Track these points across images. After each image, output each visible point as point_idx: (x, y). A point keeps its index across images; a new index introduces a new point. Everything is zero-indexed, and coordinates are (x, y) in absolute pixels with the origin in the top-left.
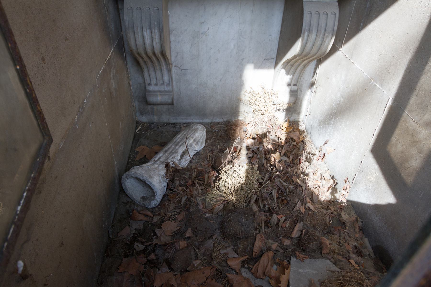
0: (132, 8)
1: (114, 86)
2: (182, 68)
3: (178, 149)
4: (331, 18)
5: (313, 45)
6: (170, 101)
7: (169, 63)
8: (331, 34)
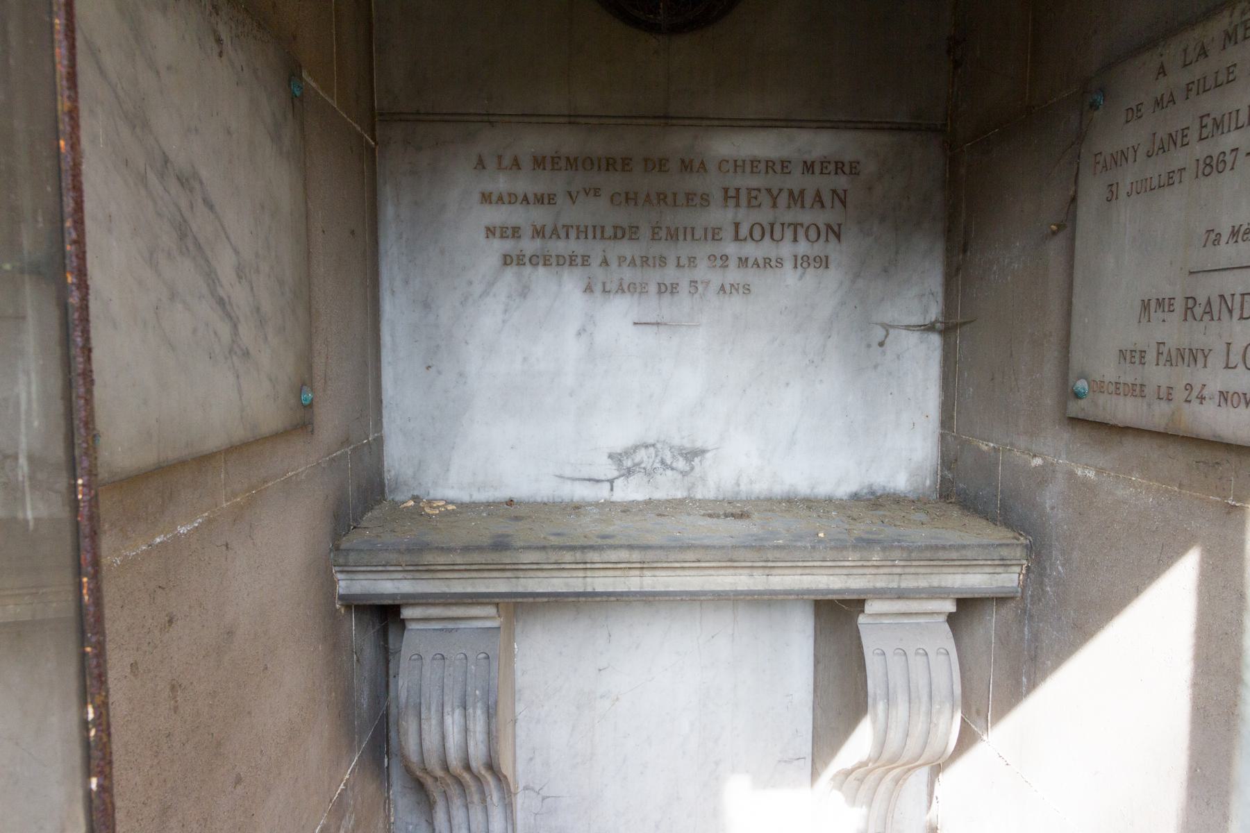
7: (509, 791)
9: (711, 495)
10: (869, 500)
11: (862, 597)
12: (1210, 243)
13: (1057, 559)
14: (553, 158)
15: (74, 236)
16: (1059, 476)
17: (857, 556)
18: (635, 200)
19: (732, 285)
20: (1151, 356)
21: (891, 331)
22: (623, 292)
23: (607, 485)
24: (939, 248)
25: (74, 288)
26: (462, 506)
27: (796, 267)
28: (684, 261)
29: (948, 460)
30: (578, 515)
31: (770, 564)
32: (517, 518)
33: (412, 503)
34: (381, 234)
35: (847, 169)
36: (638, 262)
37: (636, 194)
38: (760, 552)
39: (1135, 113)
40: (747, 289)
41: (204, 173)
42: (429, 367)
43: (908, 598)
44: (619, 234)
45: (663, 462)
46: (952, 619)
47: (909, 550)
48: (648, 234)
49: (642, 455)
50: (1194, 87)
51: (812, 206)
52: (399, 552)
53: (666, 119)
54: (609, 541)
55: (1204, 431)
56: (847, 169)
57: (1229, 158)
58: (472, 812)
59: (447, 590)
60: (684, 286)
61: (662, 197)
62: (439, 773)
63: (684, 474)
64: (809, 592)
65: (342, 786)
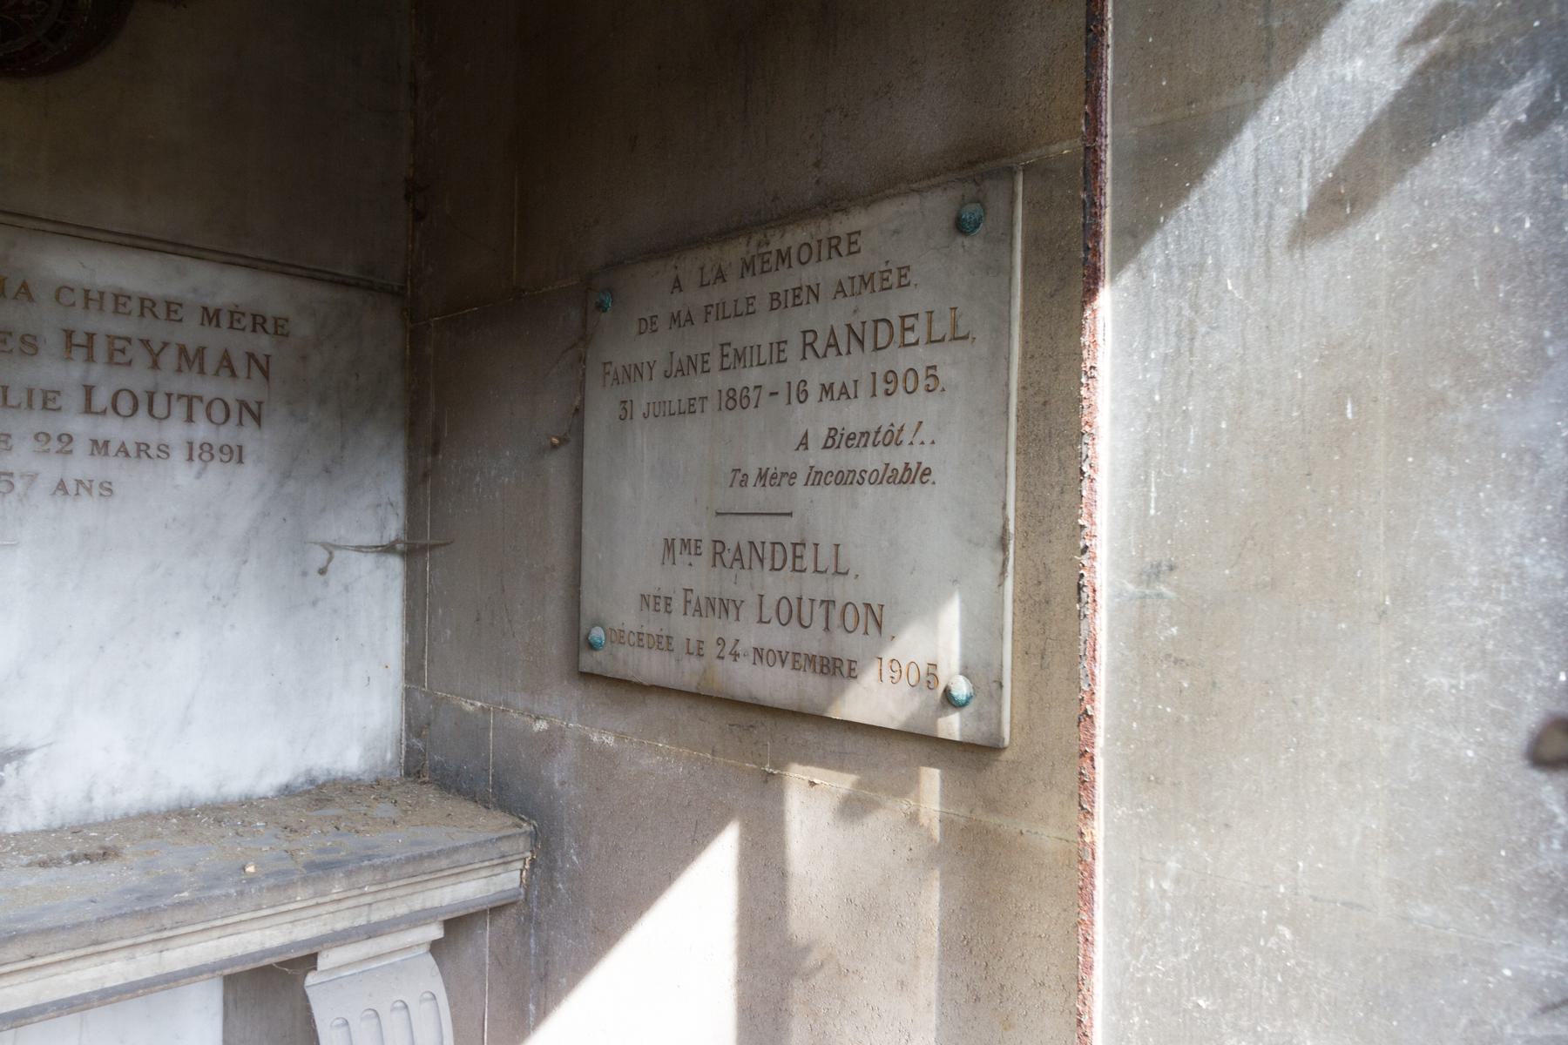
9: (38, 823)
10: (309, 792)
12: (736, 484)
13: (569, 847)
16: (570, 742)
17: (310, 890)
19: (79, 482)
20: (677, 604)
21: (337, 553)
24: (399, 444)
27: (190, 459)
29: (416, 724)
35: (269, 326)
38: (148, 913)
39: (649, 325)
47: (384, 868)
51: (217, 374)
55: (740, 693)
56: (269, 326)
57: (753, 395)
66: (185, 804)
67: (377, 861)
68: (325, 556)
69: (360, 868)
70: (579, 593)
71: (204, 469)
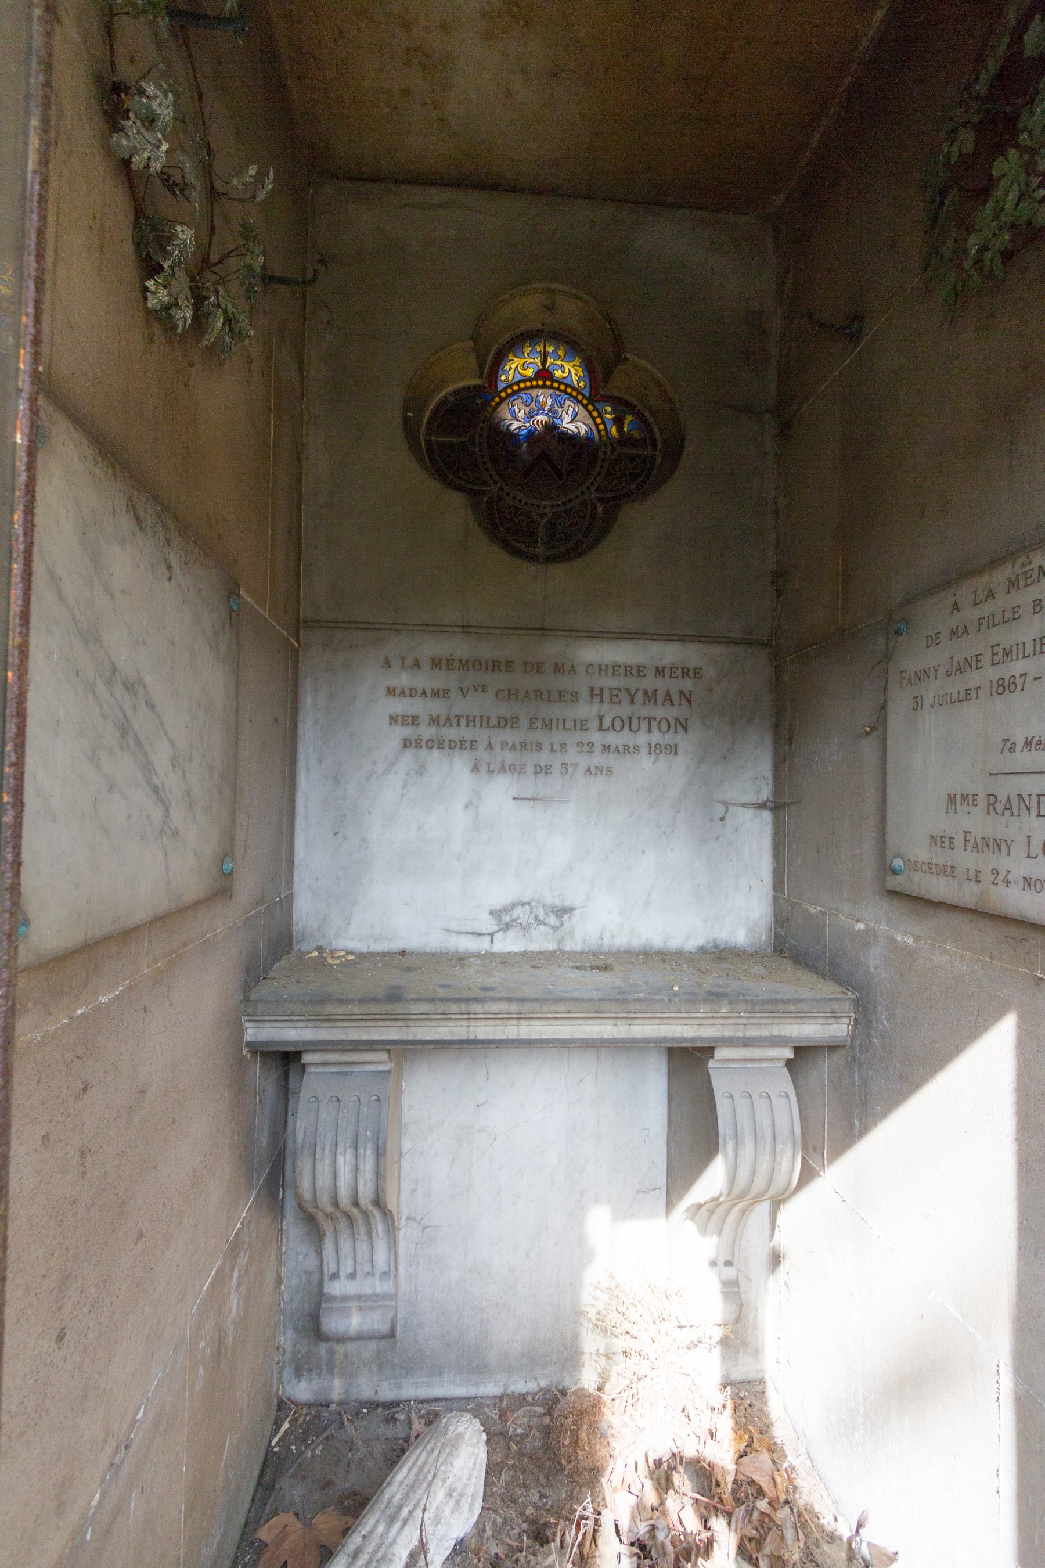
0: (318, 1100)
1: (235, 1308)
2: (425, 1222)
3: (394, 1542)
4: (779, 1104)
5: (754, 1172)
6: (385, 1328)
8: (790, 1145)
9: (578, 947)
10: (714, 953)
11: (713, 1045)
12: (1006, 750)
13: (882, 1014)
14: (448, 660)
15: (13, 758)
17: (708, 1008)
18: (517, 696)
19: (597, 768)
20: (959, 842)
22: (505, 771)
23: (488, 938)
25: (9, 807)
26: (362, 957)
27: (650, 753)
28: (556, 747)
29: (781, 918)
30: (462, 966)
31: (632, 1015)
32: (409, 969)
33: (316, 954)
34: (300, 719)
35: (691, 674)
36: (518, 747)
37: (517, 691)
38: (621, 1003)
39: (934, 640)
40: (610, 771)
41: (148, 679)
42: (336, 834)
43: (752, 1046)
44: (502, 724)
45: (536, 918)
46: (789, 1063)
48: (527, 724)
49: (518, 912)
50: (985, 622)
52: (303, 1002)
53: (543, 631)
54: (491, 994)
55: (1012, 911)
56: (691, 674)
57: (1019, 681)
58: (358, 1243)
59: (345, 1038)
60: (557, 767)
61: (539, 694)
62: (330, 1209)
63: (555, 929)
64: (665, 1040)
65: (239, 1225)
66: (648, 949)
67: (749, 998)
68: (724, 809)
69: (738, 1000)
70: (884, 834)
71: (657, 758)
